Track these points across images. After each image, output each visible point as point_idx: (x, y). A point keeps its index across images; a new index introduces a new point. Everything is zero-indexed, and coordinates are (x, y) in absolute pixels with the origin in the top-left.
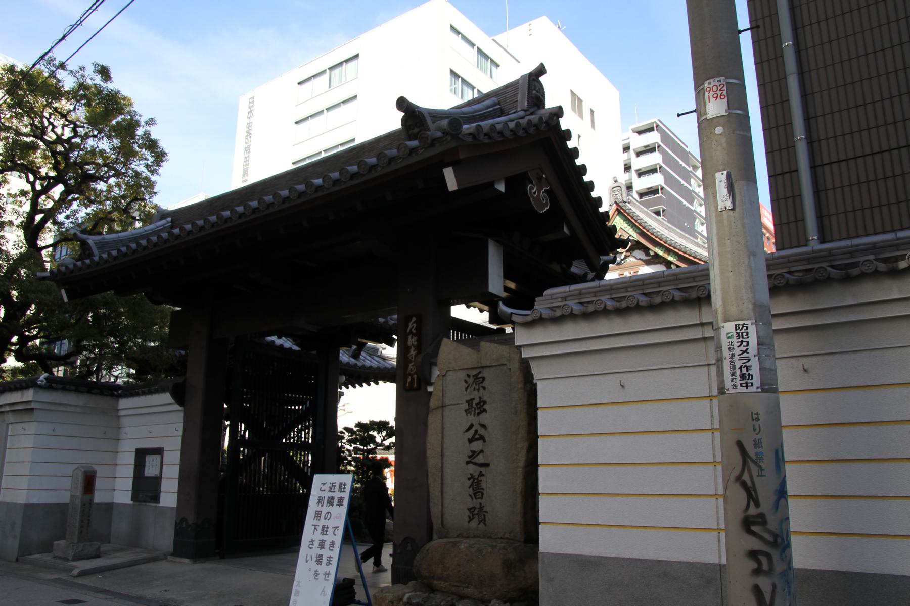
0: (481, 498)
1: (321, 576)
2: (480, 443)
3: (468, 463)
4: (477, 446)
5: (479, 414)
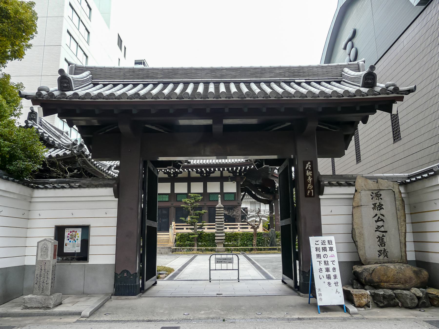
0: (385, 246)
1: (333, 285)
2: (382, 222)
3: (376, 231)
4: (380, 224)
5: (379, 210)
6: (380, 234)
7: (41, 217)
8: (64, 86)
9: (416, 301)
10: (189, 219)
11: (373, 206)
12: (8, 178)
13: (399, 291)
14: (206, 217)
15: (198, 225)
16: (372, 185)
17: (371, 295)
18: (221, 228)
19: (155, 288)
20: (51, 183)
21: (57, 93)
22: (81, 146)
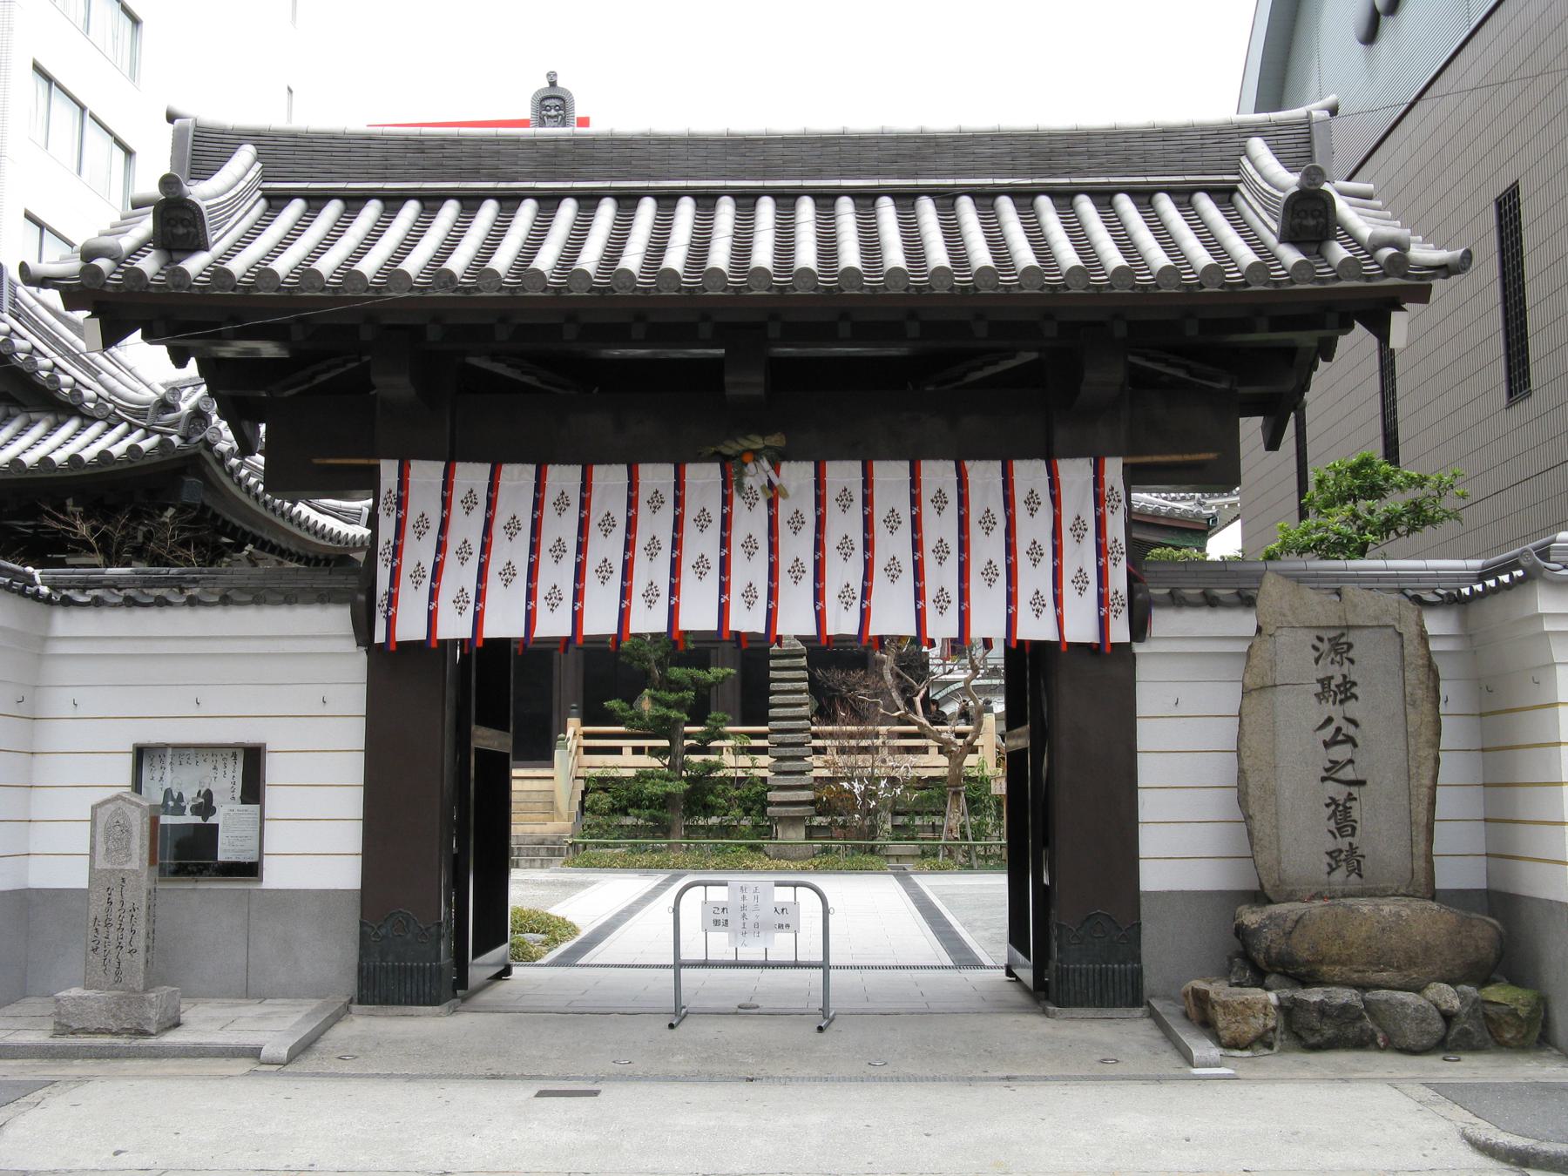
0: (1353, 835)
3: (1324, 779)
4: (1341, 752)
5: (1341, 702)
6: (1339, 792)
7: (80, 713)
8: (173, 235)
9: (1438, 1025)
10: (646, 705)
11: (1318, 688)
12: (24, 588)
13: (1383, 994)
14: (732, 696)
15: (688, 736)
16: (1319, 609)
17: (1280, 1007)
18: (797, 751)
19: (502, 987)
20: (115, 585)
21: (149, 264)
22: (198, 415)
